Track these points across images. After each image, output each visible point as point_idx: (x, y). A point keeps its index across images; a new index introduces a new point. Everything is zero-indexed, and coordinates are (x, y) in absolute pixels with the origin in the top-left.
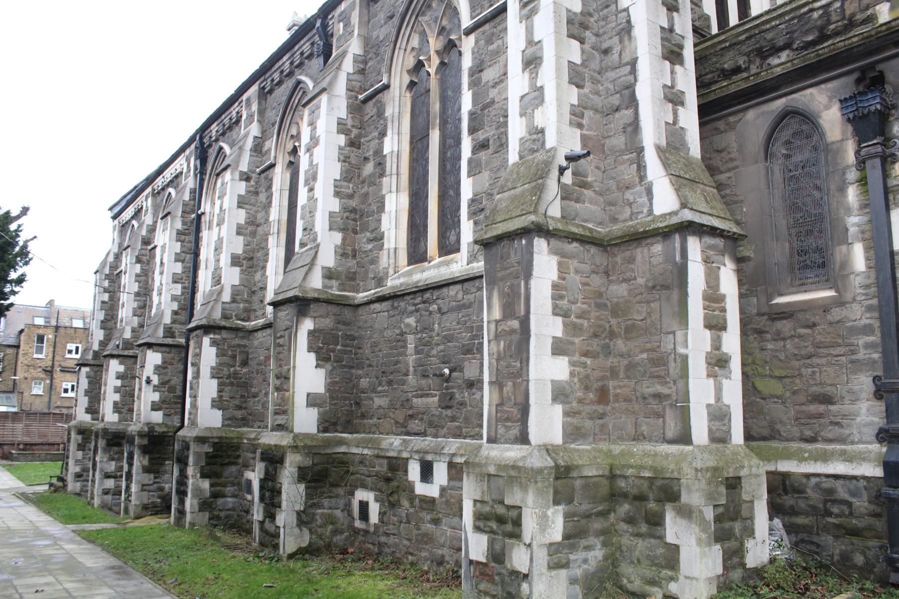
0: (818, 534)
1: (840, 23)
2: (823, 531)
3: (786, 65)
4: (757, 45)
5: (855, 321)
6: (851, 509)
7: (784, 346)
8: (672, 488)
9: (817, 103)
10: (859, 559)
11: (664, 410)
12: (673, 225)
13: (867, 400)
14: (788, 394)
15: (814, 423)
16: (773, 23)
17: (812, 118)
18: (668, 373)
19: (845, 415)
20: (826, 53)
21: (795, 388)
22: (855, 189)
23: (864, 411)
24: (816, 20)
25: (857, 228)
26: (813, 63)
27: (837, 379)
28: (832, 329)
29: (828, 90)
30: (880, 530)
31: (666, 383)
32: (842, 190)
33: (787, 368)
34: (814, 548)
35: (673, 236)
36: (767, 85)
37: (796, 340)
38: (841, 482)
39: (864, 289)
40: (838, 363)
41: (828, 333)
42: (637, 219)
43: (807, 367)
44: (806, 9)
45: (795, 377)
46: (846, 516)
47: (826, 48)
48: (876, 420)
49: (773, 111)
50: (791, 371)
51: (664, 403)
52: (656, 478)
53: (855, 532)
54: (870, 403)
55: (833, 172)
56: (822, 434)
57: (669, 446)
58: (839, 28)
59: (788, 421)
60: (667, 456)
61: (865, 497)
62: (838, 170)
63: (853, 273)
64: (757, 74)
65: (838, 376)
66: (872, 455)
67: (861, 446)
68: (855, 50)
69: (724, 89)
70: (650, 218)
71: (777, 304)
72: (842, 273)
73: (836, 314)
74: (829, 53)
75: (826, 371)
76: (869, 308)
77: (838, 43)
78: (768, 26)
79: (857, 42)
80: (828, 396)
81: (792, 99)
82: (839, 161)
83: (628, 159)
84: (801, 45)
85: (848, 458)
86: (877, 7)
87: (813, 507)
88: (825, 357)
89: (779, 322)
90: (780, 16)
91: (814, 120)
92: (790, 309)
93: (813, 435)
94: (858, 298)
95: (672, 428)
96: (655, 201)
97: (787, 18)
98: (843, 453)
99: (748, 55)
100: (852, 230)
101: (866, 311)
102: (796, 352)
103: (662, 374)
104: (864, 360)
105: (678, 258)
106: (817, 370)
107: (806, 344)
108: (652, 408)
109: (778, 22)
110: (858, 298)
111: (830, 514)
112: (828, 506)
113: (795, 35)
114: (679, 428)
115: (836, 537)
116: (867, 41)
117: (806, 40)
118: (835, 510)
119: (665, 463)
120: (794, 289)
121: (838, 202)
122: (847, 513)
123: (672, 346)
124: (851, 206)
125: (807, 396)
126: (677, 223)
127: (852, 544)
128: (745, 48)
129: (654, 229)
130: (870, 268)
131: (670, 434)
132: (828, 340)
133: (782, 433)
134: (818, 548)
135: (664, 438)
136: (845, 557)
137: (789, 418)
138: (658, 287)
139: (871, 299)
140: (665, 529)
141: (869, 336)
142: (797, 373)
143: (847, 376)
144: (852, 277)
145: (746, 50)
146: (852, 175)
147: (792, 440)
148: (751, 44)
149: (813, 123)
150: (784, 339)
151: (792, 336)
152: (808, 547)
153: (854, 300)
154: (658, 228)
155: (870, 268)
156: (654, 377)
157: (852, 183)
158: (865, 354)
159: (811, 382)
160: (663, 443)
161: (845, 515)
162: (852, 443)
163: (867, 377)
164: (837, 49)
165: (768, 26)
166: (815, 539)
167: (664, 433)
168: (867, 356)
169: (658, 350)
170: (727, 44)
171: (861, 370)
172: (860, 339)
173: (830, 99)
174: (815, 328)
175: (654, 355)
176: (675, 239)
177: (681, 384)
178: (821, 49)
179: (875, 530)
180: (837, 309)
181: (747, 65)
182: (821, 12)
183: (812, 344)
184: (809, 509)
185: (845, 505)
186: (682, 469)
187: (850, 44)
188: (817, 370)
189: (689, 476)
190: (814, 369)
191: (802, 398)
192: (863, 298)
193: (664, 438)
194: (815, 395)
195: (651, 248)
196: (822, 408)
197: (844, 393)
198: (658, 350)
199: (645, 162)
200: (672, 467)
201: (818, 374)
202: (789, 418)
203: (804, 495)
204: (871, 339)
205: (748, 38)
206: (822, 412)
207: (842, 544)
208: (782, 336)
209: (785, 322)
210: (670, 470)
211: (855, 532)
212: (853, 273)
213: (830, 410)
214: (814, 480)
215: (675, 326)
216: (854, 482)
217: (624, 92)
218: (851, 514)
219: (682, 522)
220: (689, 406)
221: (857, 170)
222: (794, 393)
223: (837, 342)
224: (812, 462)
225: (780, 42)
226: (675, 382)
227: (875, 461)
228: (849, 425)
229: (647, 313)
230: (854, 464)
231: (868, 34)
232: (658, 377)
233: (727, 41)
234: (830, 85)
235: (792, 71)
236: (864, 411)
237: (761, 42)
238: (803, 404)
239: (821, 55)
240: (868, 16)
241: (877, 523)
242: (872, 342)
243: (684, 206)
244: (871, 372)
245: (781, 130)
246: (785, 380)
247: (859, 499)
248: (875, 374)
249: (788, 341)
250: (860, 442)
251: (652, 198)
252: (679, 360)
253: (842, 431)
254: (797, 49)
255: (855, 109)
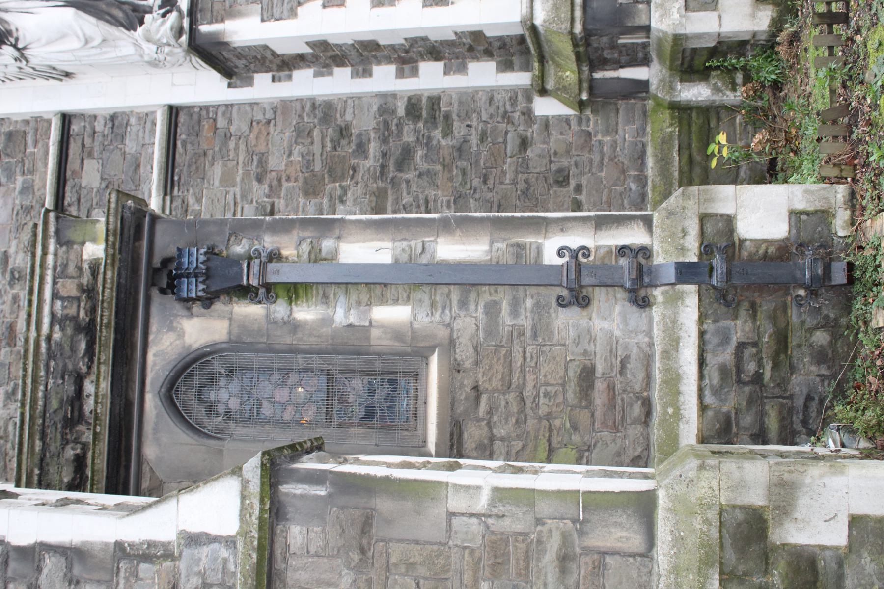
0: (791, 397)
1: (82, 304)
2: (786, 390)
3: (102, 374)
4: (59, 426)
5: (477, 326)
6: (748, 343)
7: (502, 439)
8: (739, 525)
9: (170, 348)
10: (821, 338)
11: (587, 551)
12: (262, 484)
13: (590, 319)
14: (576, 438)
15: (622, 400)
16: (40, 394)
17: (187, 359)
18: (520, 534)
19: (611, 351)
20: (110, 315)
21: (568, 425)
22: (299, 308)
23: (606, 325)
24: (64, 335)
25: (352, 311)
26: (116, 340)
27: (558, 359)
28: (486, 361)
29: (158, 331)
30: (774, 304)
31: (539, 542)
32: (294, 326)
33: (536, 438)
34: (814, 405)
35: (283, 498)
36: (117, 411)
37: (495, 418)
38: (709, 357)
39: (436, 310)
40: (535, 356)
41: (491, 367)
42: (234, 574)
43: (537, 405)
44: (43, 345)
45: (550, 426)
46: (760, 352)
47: (107, 336)
48: (618, 308)
49: (157, 416)
50: (541, 432)
51: (578, 550)
52: (721, 564)
53: (782, 340)
54: (594, 316)
55: (268, 336)
56: (638, 388)
57: (659, 543)
58: (88, 306)
59: (619, 441)
60: (678, 541)
61: (729, 323)
62: (267, 329)
63: (411, 323)
64: (96, 435)
65: (554, 358)
66: (669, 312)
67: (656, 332)
68: (123, 281)
69: (96, 478)
70: (240, 545)
71: (437, 445)
72: (408, 339)
73: (464, 353)
74: (111, 311)
75: (545, 376)
76: (463, 304)
77: (106, 316)
78: (40, 403)
79: (113, 273)
80: (582, 372)
81: (152, 383)
82: (256, 327)
83: (127, 579)
84: (86, 360)
85: (674, 342)
86: (85, 257)
87: (751, 402)
88: (525, 376)
89: (465, 446)
90: (35, 381)
91: (192, 356)
92: (448, 425)
93: (639, 402)
94: (447, 319)
95: (624, 534)
96: (214, 531)
97: (42, 373)
98: (666, 355)
99: (65, 442)
100: (353, 318)
101: (467, 310)
102: (514, 420)
103: (522, 546)
104: (533, 319)
105: (321, 491)
106: (542, 390)
107: (503, 403)
108: (585, 578)
109: (42, 388)
110: (447, 319)
111: (758, 378)
112: (747, 379)
113: (70, 367)
114: (623, 519)
115: (792, 369)
116: (117, 264)
117: (82, 352)
118: (751, 367)
119: (692, 541)
120: (420, 427)
121: (311, 335)
122: (754, 350)
123: (474, 520)
124: (320, 317)
125: (581, 407)
126: (262, 476)
127: (799, 346)
128: (53, 447)
129: (261, 528)
130: (408, 298)
131: (635, 541)
132: (500, 368)
133: (637, 454)
134: (813, 399)
135: (642, 555)
136: (820, 357)
137: (614, 440)
138: (365, 542)
139: (451, 300)
140: (823, 548)
141: (501, 309)
142: (545, 423)
143: (556, 345)
144: (416, 325)
145: (59, 444)
146: (280, 309)
147: (647, 438)
148: (53, 436)
149: (195, 361)
150: (492, 439)
151: (489, 425)
152: (814, 415)
153: (449, 325)
154: (261, 519)
155: (408, 298)
156: (527, 568)
157: (291, 310)
158: (526, 317)
159: (560, 399)
160: (652, 559)
161: (758, 353)
162: (651, 345)
163: (557, 316)
164: (112, 300)
165: (40, 403)
166: (800, 402)
167: (634, 555)
168: (528, 314)
169: (477, 554)
170: (37, 471)
171: (548, 325)
172: (504, 322)
173: (171, 329)
174: (481, 388)
175: (486, 562)
176: (287, 494)
177: (544, 508)
178: (101, 319)
179: (775, 311)
180: (458, 351)
181: (79, 446)
182: (57, 328)
183: (504, 394)
184: (754, 409)
185: (742, 353)
186: (701, 499)
187: (112, 283)
188: (542, 390)
189: (715, 484)
190: (541, 394)
191: (583, 417)
192: (447, 312)
193: (642, 555)
194: (580, 391)
195: (292, 549)
196: (600, 385)
197: (579, 350)
198: (477, 554)
199: (142, 543)
200: (698, 523)
201: (549, 388)
202: (614, 440)
203: (733, 416)
204: (505, 307)
205: (43, 438)
206: (605, 385)
207: (802, 360)
208: (486, 441)
209: (465, 436)
210: (705, 529)
211: (782, 340)
212: (411, 323)
213: (603, 374)
214: (709, 399)
215: (437, 512)
216: (707, 337)
217: (10, 573)
218: (755, 344)
219: (804, 505)
220: (585, 493)
221: (275, 302)
222: (575, 428)
223: (505, 355)
224: (681, 398)
225: (70, 389)
226: (539, 521)
227: (676, 307)
228: (626, 347)
229: (406, 574)
230: (682, 334)
231: (110, 257)
232: (527, 558)
233: (32, 471)
234: (154, 327)
235: (113, 370)
236: (606, 325)
237: (57, 419)
238: (593, 415)
239: (109, 323)
240: (90, 268)
241: (765, 308)
242: (510, 305)
243: (237, 471)
244: (552, 311)
245: (188, 413)
246: (555, 444)
247: (733, 332)
248: (554, 303)
249: (495, 431)
250: (649, 333)
251: (207, 534)
252: (501, 509)
253: (633, 357)
254: (89, 368)
255: (194, 280)
